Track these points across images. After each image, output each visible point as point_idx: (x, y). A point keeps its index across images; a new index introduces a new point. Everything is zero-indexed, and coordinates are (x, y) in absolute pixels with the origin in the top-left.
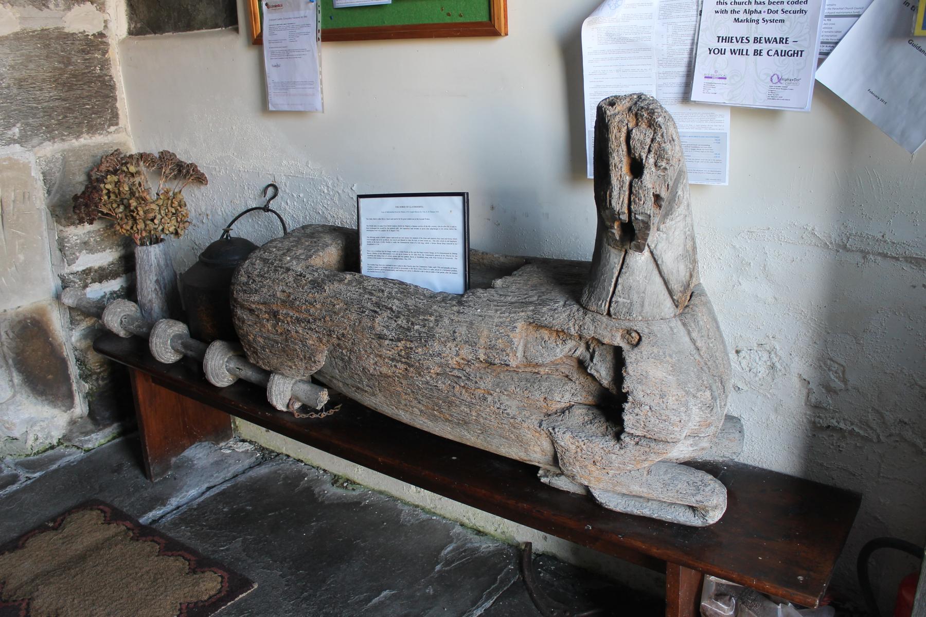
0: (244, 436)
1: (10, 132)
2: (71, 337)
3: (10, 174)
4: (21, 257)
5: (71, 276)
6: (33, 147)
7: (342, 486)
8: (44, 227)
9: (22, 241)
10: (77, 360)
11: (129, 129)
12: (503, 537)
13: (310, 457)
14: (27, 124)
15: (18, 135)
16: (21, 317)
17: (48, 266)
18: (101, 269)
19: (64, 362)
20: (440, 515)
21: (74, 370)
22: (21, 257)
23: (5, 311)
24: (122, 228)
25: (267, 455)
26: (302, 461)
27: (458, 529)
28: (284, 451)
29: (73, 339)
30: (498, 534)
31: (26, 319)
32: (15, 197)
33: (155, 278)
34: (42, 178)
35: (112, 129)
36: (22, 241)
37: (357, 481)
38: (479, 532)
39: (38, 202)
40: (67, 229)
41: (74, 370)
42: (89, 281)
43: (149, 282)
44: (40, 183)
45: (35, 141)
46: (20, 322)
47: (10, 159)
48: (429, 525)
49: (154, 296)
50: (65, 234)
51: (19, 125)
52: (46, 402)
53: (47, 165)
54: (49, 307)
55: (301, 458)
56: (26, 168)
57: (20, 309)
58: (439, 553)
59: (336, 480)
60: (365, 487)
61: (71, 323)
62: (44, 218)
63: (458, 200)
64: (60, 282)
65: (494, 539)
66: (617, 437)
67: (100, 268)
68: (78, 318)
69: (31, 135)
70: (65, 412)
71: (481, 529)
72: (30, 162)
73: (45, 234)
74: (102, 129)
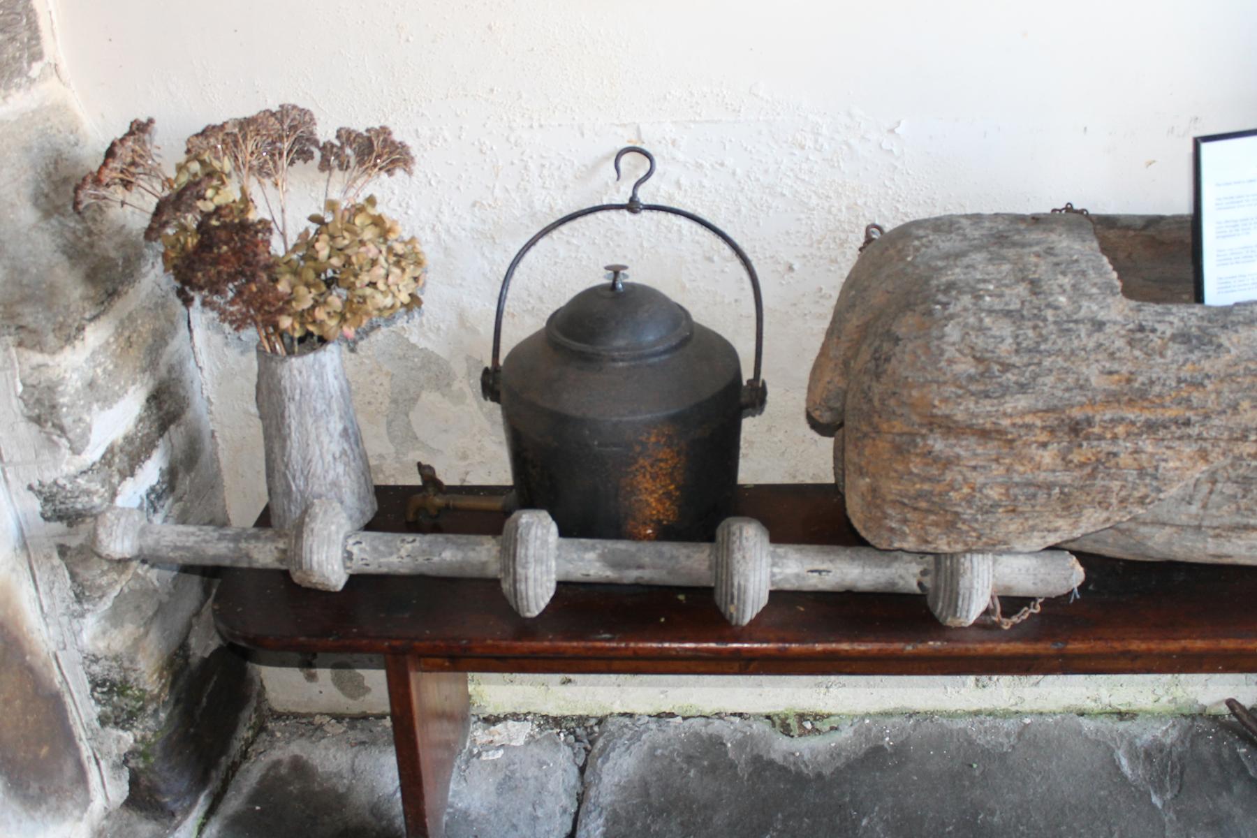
0: (490, 710)
2: (76, 634)
5: (81, 481)
7: (804, 733)
10: (95, 684)
11: (63, 67)
12: (1172, 707)
13: (692, 701)
18: (128, 439)
19: (55, 703)
20: (1032, 713)
21: (83, 710)
25: (586, 735)
26: (672, 715)
28: (618, 708)
29: (86, 637)
33: (340, 427)
35: (36, 68)
37: (825, 711)
38: (1121, 715)
40: (59, 358)
41: (83, 710)
42: (116, 480)
43: (325, 439)
48: (1036, 738)
49: (340, 469)
50: (53, 374)
52: (49, 817)
54: (14, 577)
55: (667, 709)
58: (1124, 777)
59: (782, 724)
60: (852, 717)
61: (79, 598)
63: (1205, 147)
65: (1159, 717)
66: (420, 465)
67: (126, 438)
68: (104, 581)
70: (80, 819)
71: (1123, 709)
74: (20, 72)
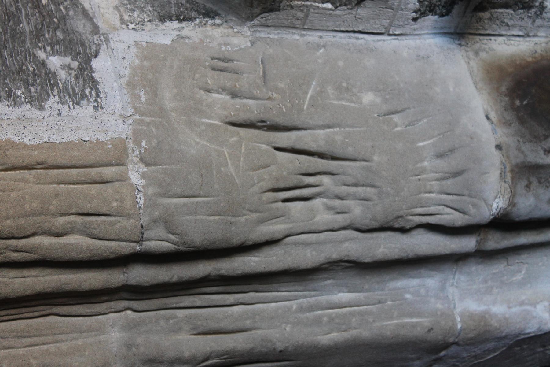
1: (62, 75)
3: (167, 96)
4: (368, 98)
6: (96, 30)
8: (294, 37)
9: (330, 90)
14: (37, 35)
15: (68, 60)
16: (509, 116)
17: (387, 43)
22: (368, 98)
23: (499, 147)
24: (34, 70)
27: (407, 30)
30: (505, 188)
31: (511, 107)
32: (224, 90)
34: (176, 24)
36: (330, 90)
39: (235, 41)
44: (189, 30)
45: (80, 25)
46: (522, 121)
47: (131, 85)
51: (41, 55)
53: (142, 9)
54: (483, 55)
56: (150, 52)
57: (492, 115)
62: (274, 34)
64: (431, 19)
69: (64, 31)
72: (136, 44)
73: (313, 37)
